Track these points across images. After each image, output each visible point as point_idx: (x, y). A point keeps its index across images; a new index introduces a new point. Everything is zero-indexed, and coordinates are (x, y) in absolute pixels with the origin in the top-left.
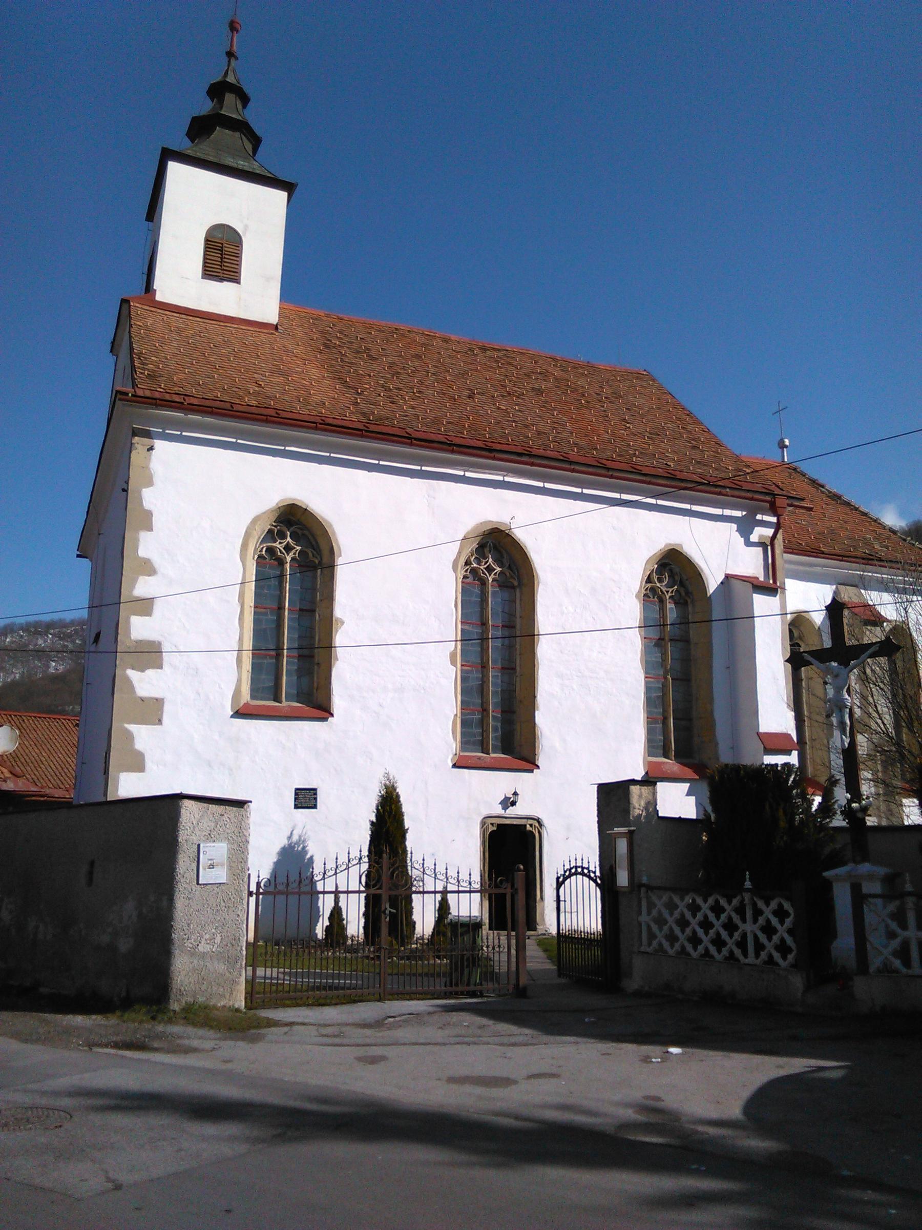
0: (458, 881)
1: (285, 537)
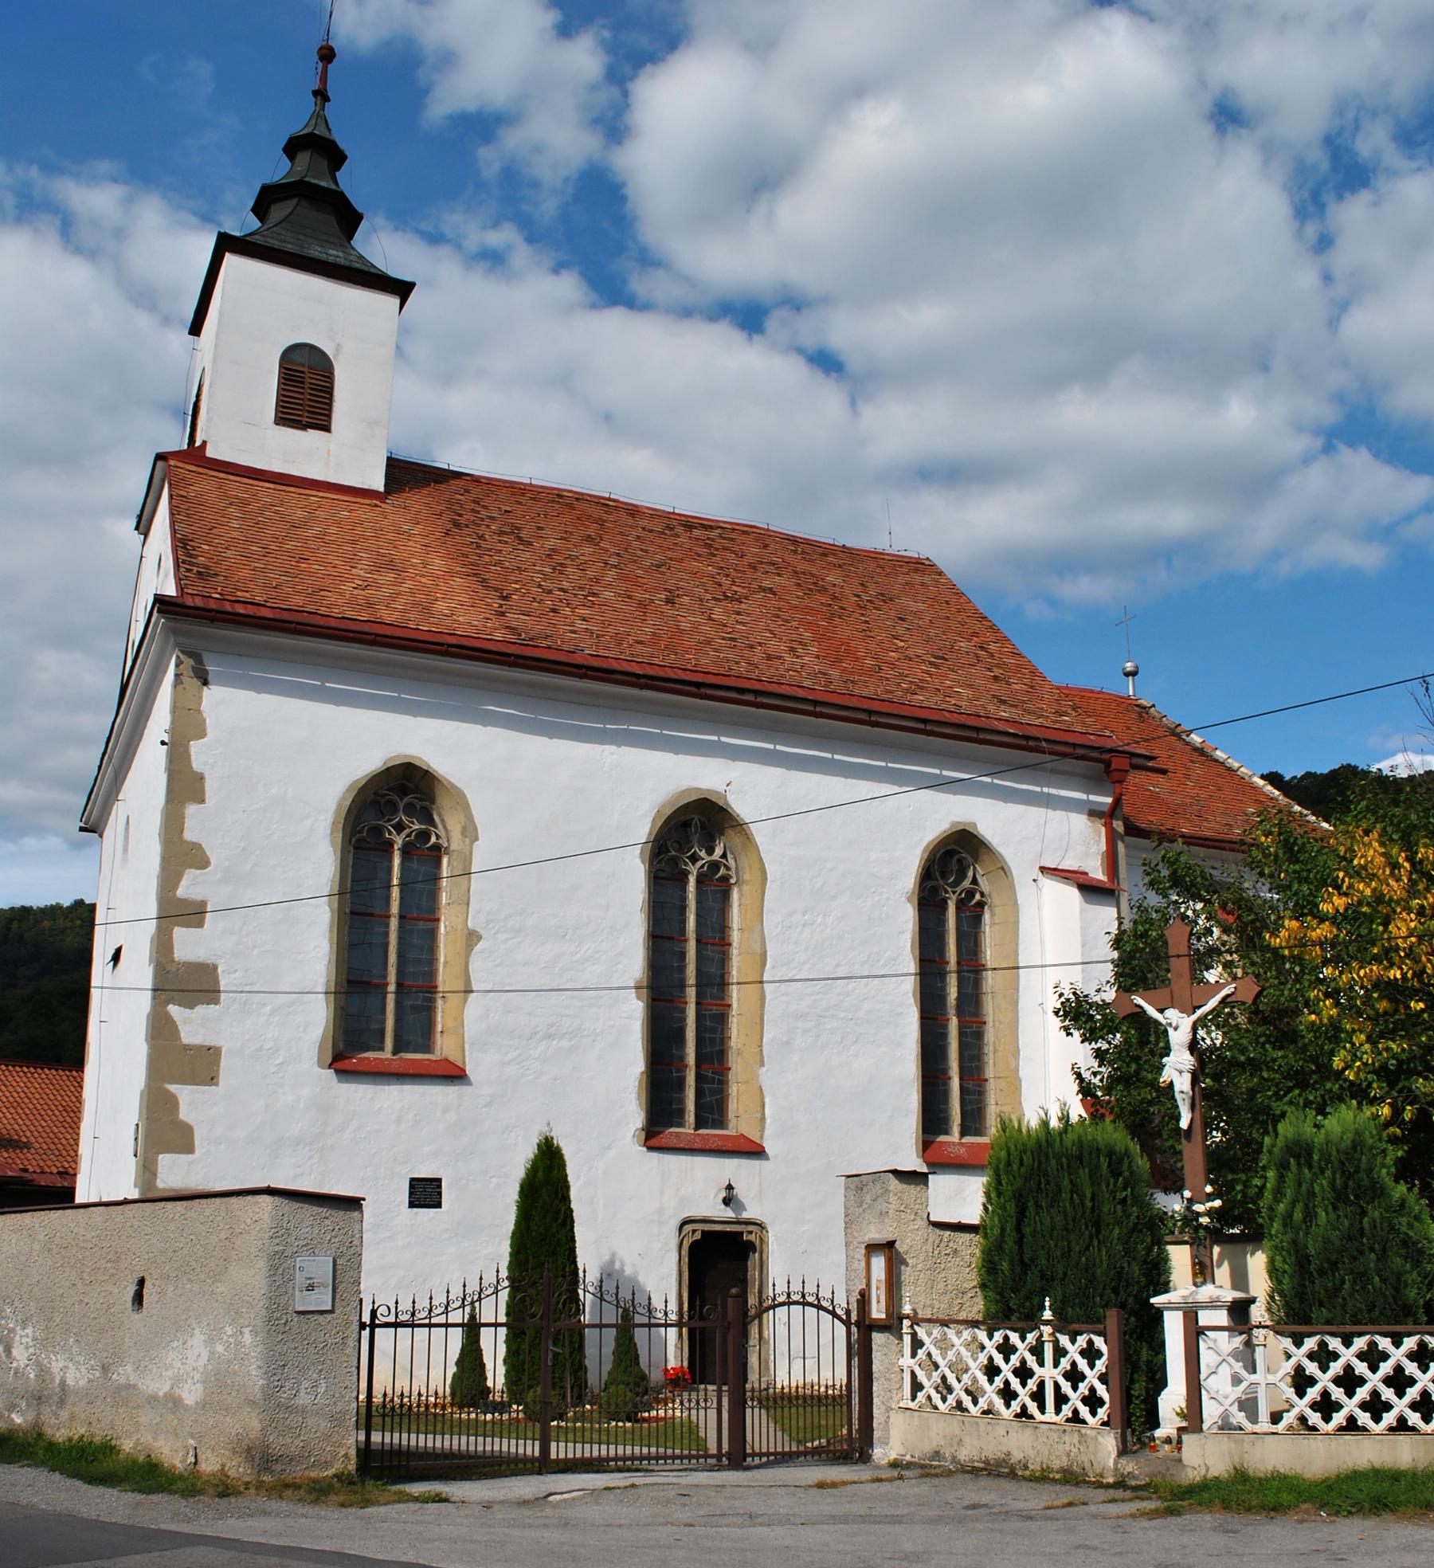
0: (650, 1311)
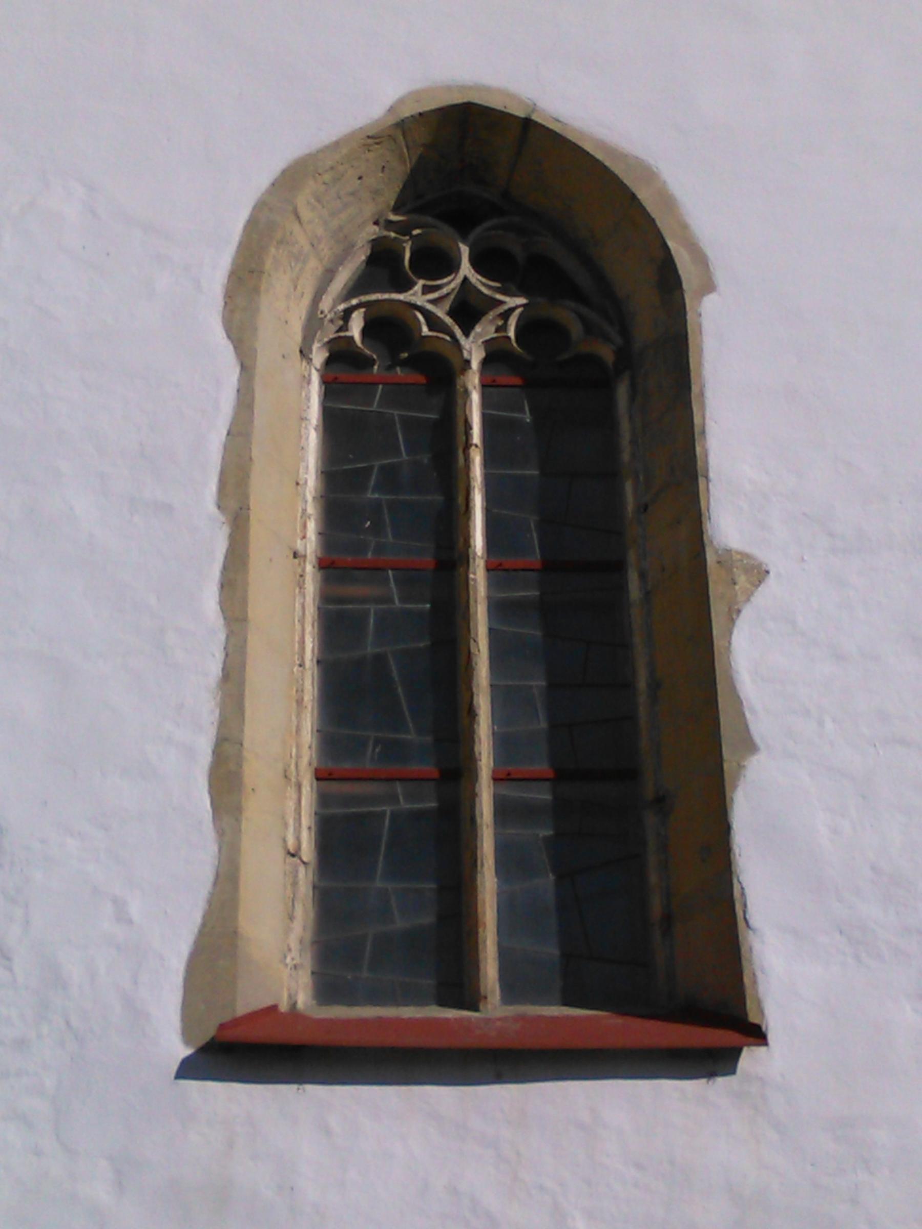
1: (449, 266)
